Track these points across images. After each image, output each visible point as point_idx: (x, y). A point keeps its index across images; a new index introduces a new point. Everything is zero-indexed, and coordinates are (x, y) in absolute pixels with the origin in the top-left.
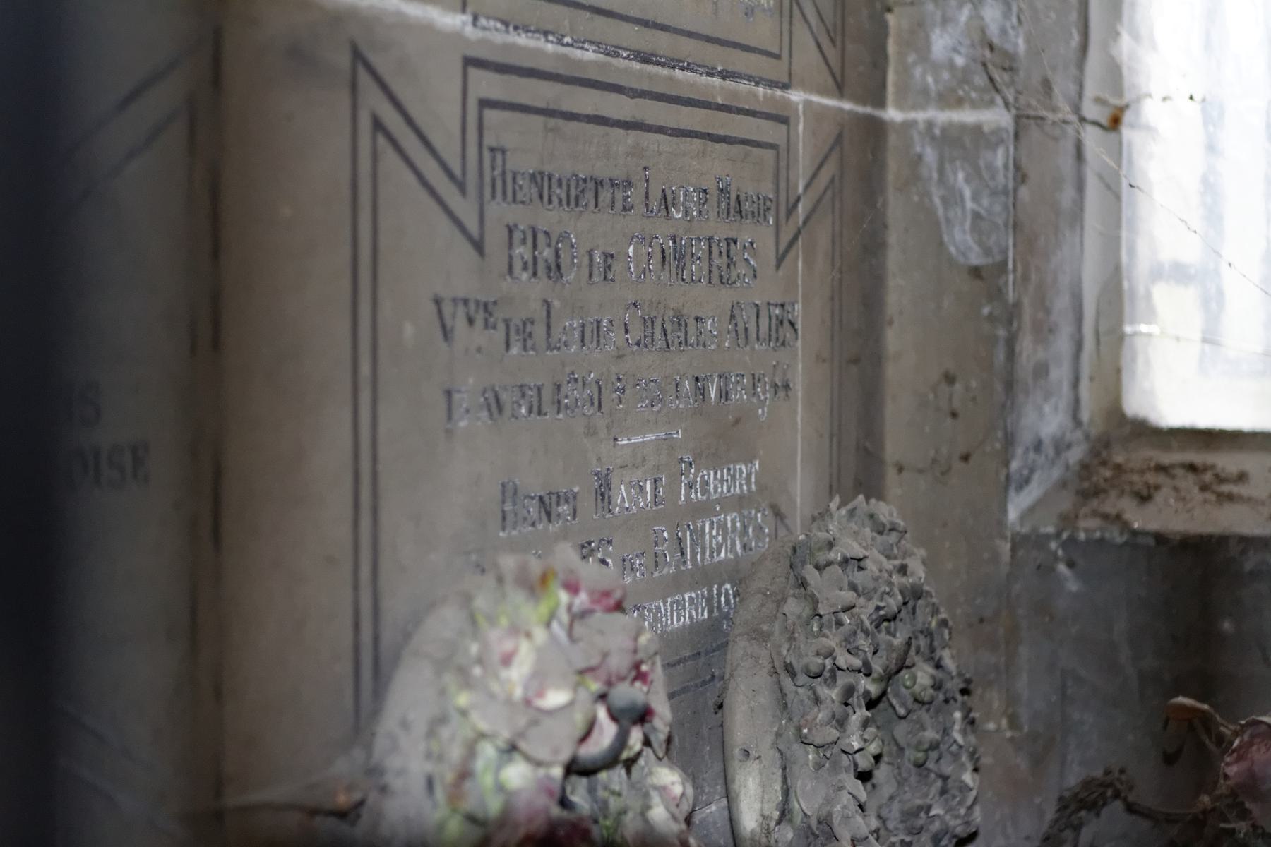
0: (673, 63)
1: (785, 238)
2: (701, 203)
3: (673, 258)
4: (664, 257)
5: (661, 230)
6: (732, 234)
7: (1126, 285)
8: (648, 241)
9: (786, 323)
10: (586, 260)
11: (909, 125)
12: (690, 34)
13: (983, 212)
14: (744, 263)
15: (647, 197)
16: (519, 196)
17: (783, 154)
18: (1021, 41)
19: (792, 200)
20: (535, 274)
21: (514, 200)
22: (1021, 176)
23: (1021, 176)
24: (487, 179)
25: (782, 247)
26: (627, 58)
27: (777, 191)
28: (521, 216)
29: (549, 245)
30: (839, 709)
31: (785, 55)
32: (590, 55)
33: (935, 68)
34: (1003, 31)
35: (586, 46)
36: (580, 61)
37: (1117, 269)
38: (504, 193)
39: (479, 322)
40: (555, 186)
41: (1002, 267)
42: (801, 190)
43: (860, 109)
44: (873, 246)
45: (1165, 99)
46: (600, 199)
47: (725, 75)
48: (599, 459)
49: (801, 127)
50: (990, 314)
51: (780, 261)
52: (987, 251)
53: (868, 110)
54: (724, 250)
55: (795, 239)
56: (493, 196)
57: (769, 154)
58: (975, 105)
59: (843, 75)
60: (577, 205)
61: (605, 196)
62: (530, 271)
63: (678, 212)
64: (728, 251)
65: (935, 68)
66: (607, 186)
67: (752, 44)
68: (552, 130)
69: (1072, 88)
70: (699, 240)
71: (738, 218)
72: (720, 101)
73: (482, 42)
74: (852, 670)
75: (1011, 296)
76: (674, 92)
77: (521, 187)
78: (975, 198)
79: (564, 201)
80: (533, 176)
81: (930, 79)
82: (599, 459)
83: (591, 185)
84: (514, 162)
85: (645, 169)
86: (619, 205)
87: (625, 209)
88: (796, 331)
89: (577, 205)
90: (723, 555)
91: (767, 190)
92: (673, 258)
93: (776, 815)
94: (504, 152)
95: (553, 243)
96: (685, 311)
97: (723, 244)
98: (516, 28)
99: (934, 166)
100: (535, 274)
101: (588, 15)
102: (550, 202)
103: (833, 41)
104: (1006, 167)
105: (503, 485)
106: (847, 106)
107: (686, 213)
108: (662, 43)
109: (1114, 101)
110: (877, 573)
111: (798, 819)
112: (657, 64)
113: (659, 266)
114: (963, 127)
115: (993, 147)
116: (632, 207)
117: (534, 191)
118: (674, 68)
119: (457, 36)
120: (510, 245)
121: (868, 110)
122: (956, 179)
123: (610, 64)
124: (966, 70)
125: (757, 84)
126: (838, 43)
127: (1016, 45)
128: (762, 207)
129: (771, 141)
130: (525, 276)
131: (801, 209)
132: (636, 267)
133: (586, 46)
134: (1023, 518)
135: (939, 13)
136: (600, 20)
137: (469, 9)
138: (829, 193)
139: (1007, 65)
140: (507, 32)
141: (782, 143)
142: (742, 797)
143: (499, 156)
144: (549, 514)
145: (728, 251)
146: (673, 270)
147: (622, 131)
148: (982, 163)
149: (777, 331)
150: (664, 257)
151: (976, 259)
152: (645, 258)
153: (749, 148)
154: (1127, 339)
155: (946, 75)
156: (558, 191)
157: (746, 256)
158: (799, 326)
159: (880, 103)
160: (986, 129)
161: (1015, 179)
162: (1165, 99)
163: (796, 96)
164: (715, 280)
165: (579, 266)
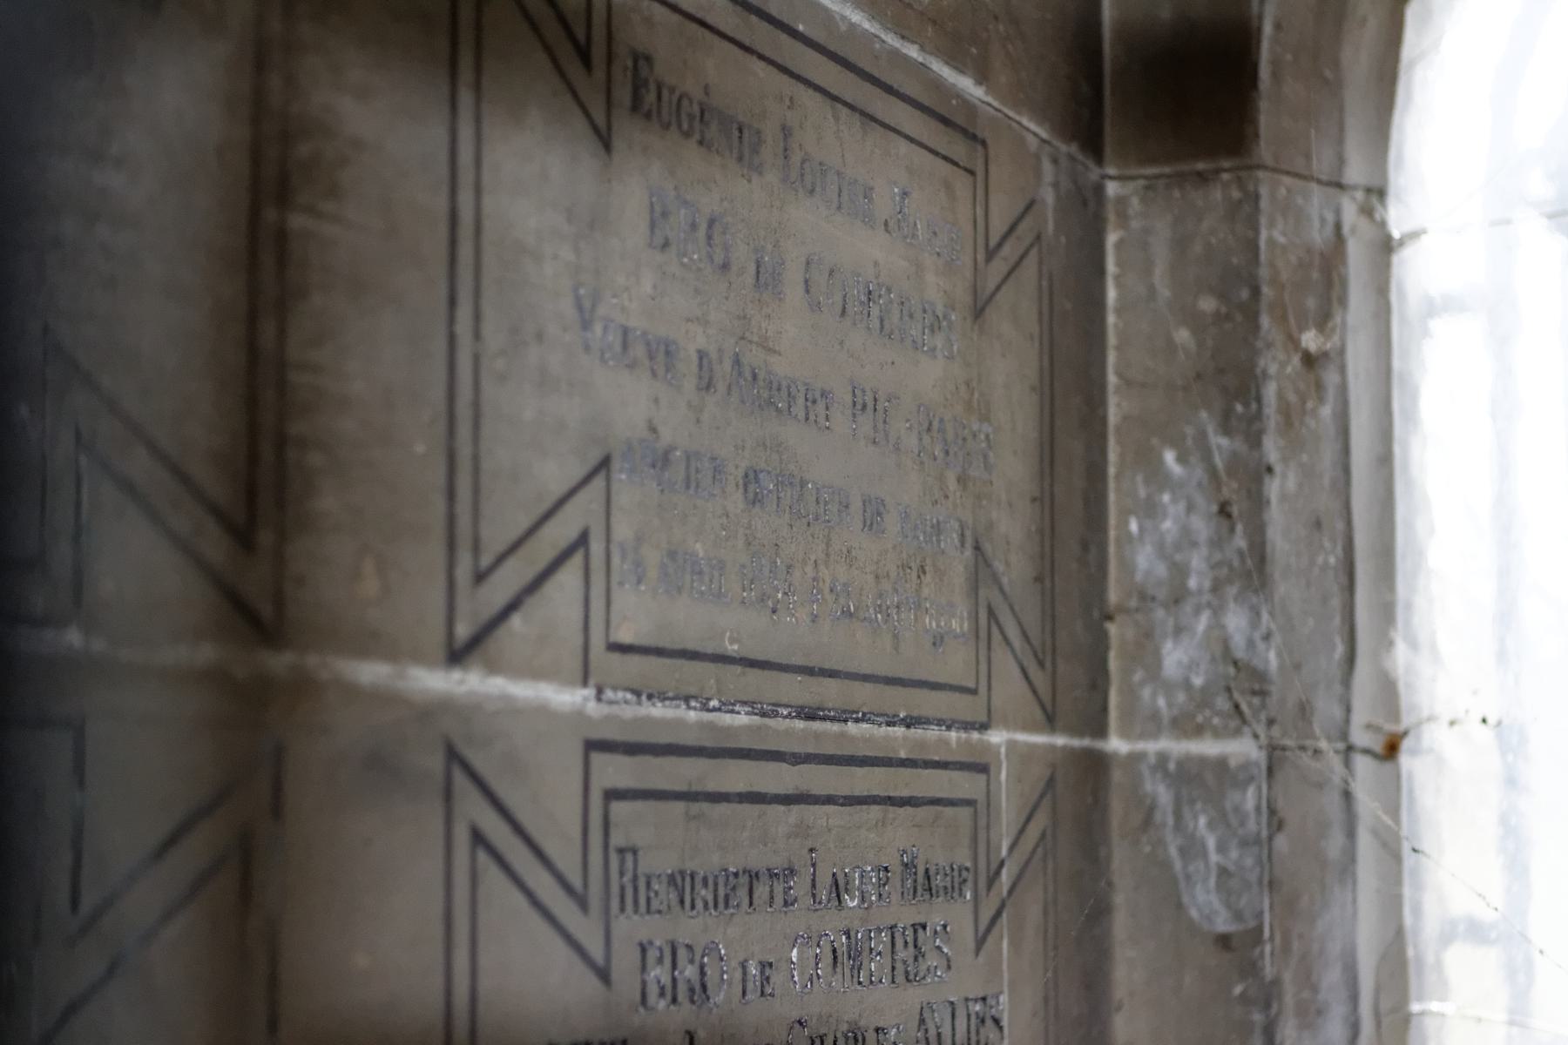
2: (882, 884)
3: (848, 958)
4: (835, 958)
5: (831, 924)
7: (1410, 952)
8: (815, 940)
10: (738, 975)
11: (1136, 758)
12: (866, 678)
13: (1232, 868)
14: (935, 953)
15: (814, 886)
16: (655, 904)
17: (981, 807)
18: (1272, 656)
19: (994, 866)
20: (674, 1000)
21: (648, 911)
22: (1276, 823)
23: (1276, 823)
24: (615, 889)
25: (982, 928)
26: (789, 716)
28: (655, 929)
29: (692, 961)
31: (983, 689)
32: (742, 719)
33: (1168, 688)
34: (1251, 644)
35: (737, 708)
37: (1399, 933)
38: (636, 902)
40: (699, 886)
41: (1256, 935)
42: (1004, 852)
43: (1076, 742)
44: (1098, 912)
45: (1452, 723)
46: (755, 896)
47: (909, 723)
50: (1243, 994)
51: (980, 943)
52: (1238, 916)
53: (1086, 742)
54: (910, 939)
55: (998, 914)
56: (622, 909)
57: (964, 813)
58: (1218, 734)
59: (1054, 705)
60: (727, 905)
61: (761, 891)
62: (669, 996)
63: (852, 899)
64: (916, 940)
65: (1168, 688)
66: (764, 878)
67: (941, 679)
69: (1337, 712)
70: (879, 930)
71: (927, 896)
72: (903, 755)
73: (608, 719)
75: (1269, 971)
76: (847, 751)
77: (656, 893)
78: (1222, 848)
79: (711, 904)
80: (672, 879)
81: (1161, 702)
83: (744, 880)
85: (811, 850)
86: (779, 900)
87: (786, 904)
88: (1001, 1029)
89: (727, 905)
91: (963, 857)
92: (848, 958)
95: (697, 958)
96: (862, 1023)
98: (650, 697)
99: (1170, 809)
100: (674, 1000)
101: (738, 669)
102: (693, 907)
103: (1041, 664)
104: (1258, 809)
106: (1060, 741)
107: (863, 900)
108: (830, 692)
109: (1390, 727)
112: (824, 719)
113: (830, 969)
114: (1203, 761)
115: (1242, 785)
116: (796, 900)
117: (673, 896)
118: (846, 721)
119: (579, 715)
120: (644, 968)
121: (1086, 742)
122: (1196, 827)
123: (768, 727)
124: (1204, 689)
125: (949, 728)
126: (1048, 664)
127: (1267, 661)
128: (956, 880)
129: (967, 796)
130: (662, 1004)
131: (1005, 878)
132: (801, 974)
133: (737, 708)
135: (1171, 622)
136: (754, 675)
137: (592, 681)
139: (1257, 687)
140: (639, 703)
141: (980, 796)
143: (629, 857)
145: (916, 940)
146: (847, 971)
147: (782, 808)
148: (1228, 805)
149: (978, 1032)
150: (835, 958)
151: (1223, 924)
152: (813, 961)
153: (939, 808)
154: (1414, 1022)
155: (1181, 697)
156: (703, 892)
157: (938, 942)
158: (1005, 1023)
159: (1101, 731)
160: (1233, 763)
161: (1269, 825)
162: (1452, 723)
164: (900, 978)
165: (730, 983)
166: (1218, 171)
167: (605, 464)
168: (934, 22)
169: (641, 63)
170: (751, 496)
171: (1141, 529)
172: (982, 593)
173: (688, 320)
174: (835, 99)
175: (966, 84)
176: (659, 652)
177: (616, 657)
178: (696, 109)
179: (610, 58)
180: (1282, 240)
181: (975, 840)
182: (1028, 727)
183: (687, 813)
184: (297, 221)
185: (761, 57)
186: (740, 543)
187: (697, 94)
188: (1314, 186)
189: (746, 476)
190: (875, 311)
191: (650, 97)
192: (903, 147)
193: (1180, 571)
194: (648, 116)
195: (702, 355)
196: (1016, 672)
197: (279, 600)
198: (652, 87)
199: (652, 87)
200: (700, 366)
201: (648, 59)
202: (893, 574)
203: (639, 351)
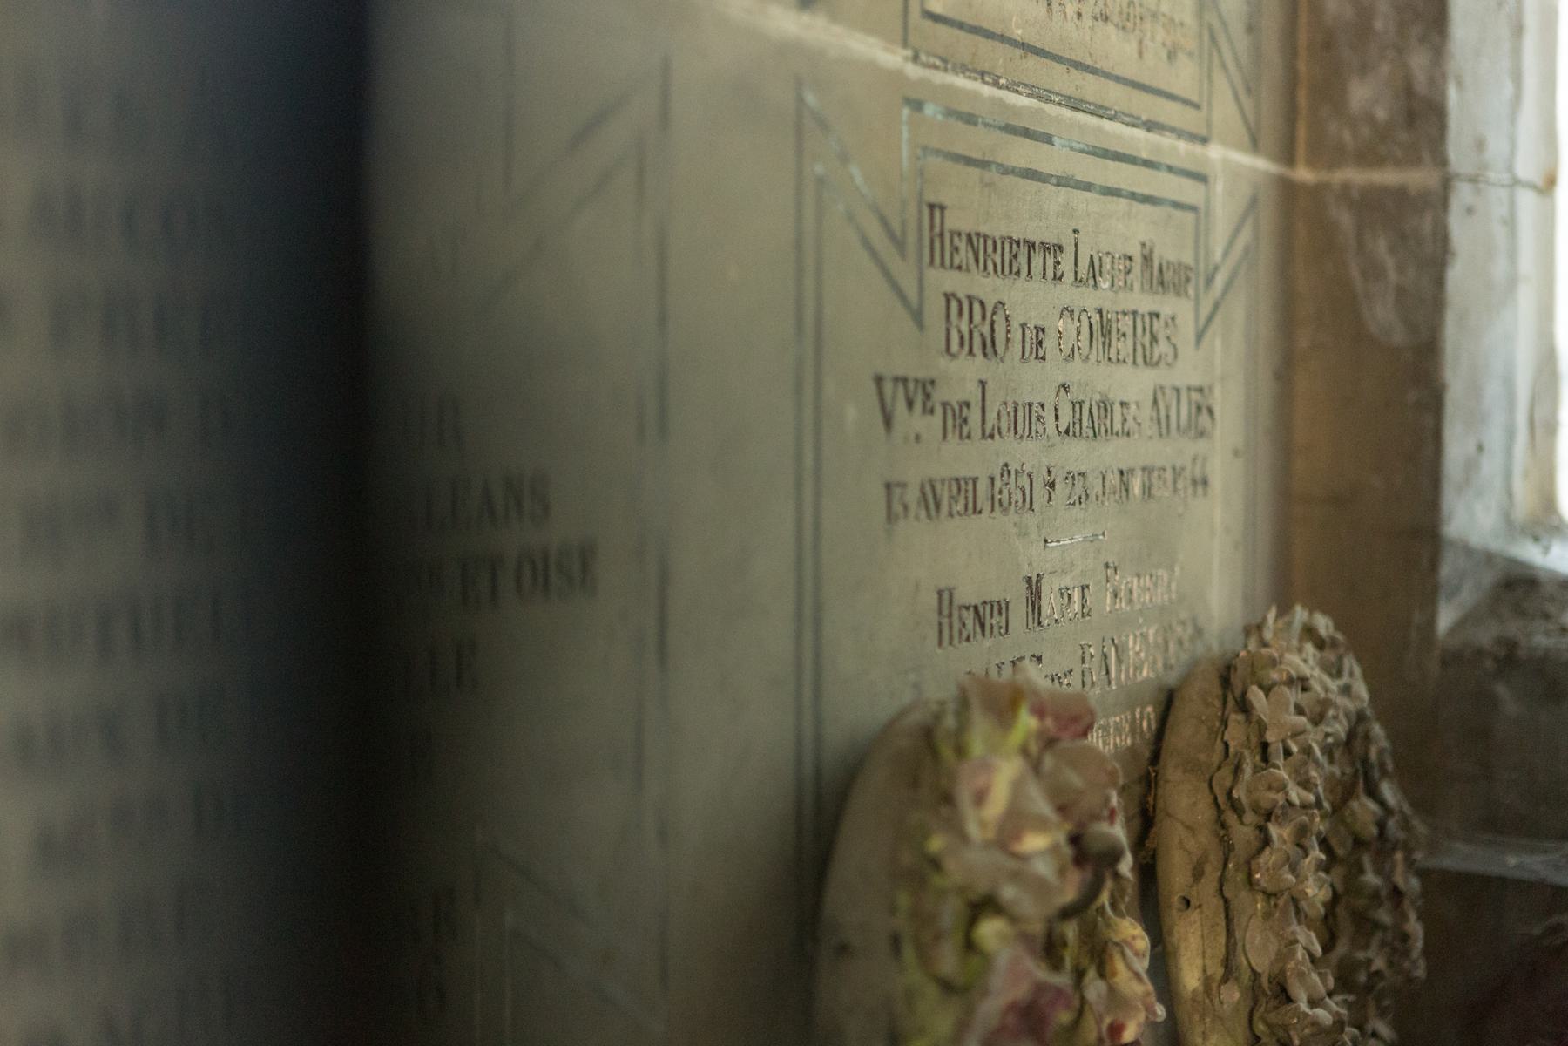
0: (1099, 111)
1: (1205, 311)
5: (1087, 299)
6: (1155, 308)
9: (1205, 411)
12: (1118, 79)
20: (971, 351)
27: (1197, 260)
30: (1290, 848)
31: (1205, 105)
36: (1014, 106)
39: (918, 406)
42: (1218, 253)
48: (1030, 564)
51: (1199, 337)
57: (1189, 217)
58: (1398, 163)
61: (1037, 260)
68: (987, 185)
72: (1144, 155)
74: (1305, 806)
78: (1401, 269)
81: (1347, 136)
82: (1030, 564)
84: (954, 221)
90: (1145, 673)
91: (1187, 258)
93: (1220, 971)
94: (942, 208)
96: (1111, 396)
97: (1147, 319)
103: (1249, 90)
105: (940, 593)
110: (1323, 695)
111: (1246, 977)
114: (1385, 190)
119: (896, 76)
129: (1172, 177)
131: (1220, 281)
134: (1460, 625)
140: (946, 70)
141: (1200, 203)
142: (1182, 951)
144: (983, 626)
155: (1365, 131)
176: (961, 26)
177: (928, 23)
181: (1197, 242)
182: (1238, 147)
183: (981, 180)
196: (1229, 93)
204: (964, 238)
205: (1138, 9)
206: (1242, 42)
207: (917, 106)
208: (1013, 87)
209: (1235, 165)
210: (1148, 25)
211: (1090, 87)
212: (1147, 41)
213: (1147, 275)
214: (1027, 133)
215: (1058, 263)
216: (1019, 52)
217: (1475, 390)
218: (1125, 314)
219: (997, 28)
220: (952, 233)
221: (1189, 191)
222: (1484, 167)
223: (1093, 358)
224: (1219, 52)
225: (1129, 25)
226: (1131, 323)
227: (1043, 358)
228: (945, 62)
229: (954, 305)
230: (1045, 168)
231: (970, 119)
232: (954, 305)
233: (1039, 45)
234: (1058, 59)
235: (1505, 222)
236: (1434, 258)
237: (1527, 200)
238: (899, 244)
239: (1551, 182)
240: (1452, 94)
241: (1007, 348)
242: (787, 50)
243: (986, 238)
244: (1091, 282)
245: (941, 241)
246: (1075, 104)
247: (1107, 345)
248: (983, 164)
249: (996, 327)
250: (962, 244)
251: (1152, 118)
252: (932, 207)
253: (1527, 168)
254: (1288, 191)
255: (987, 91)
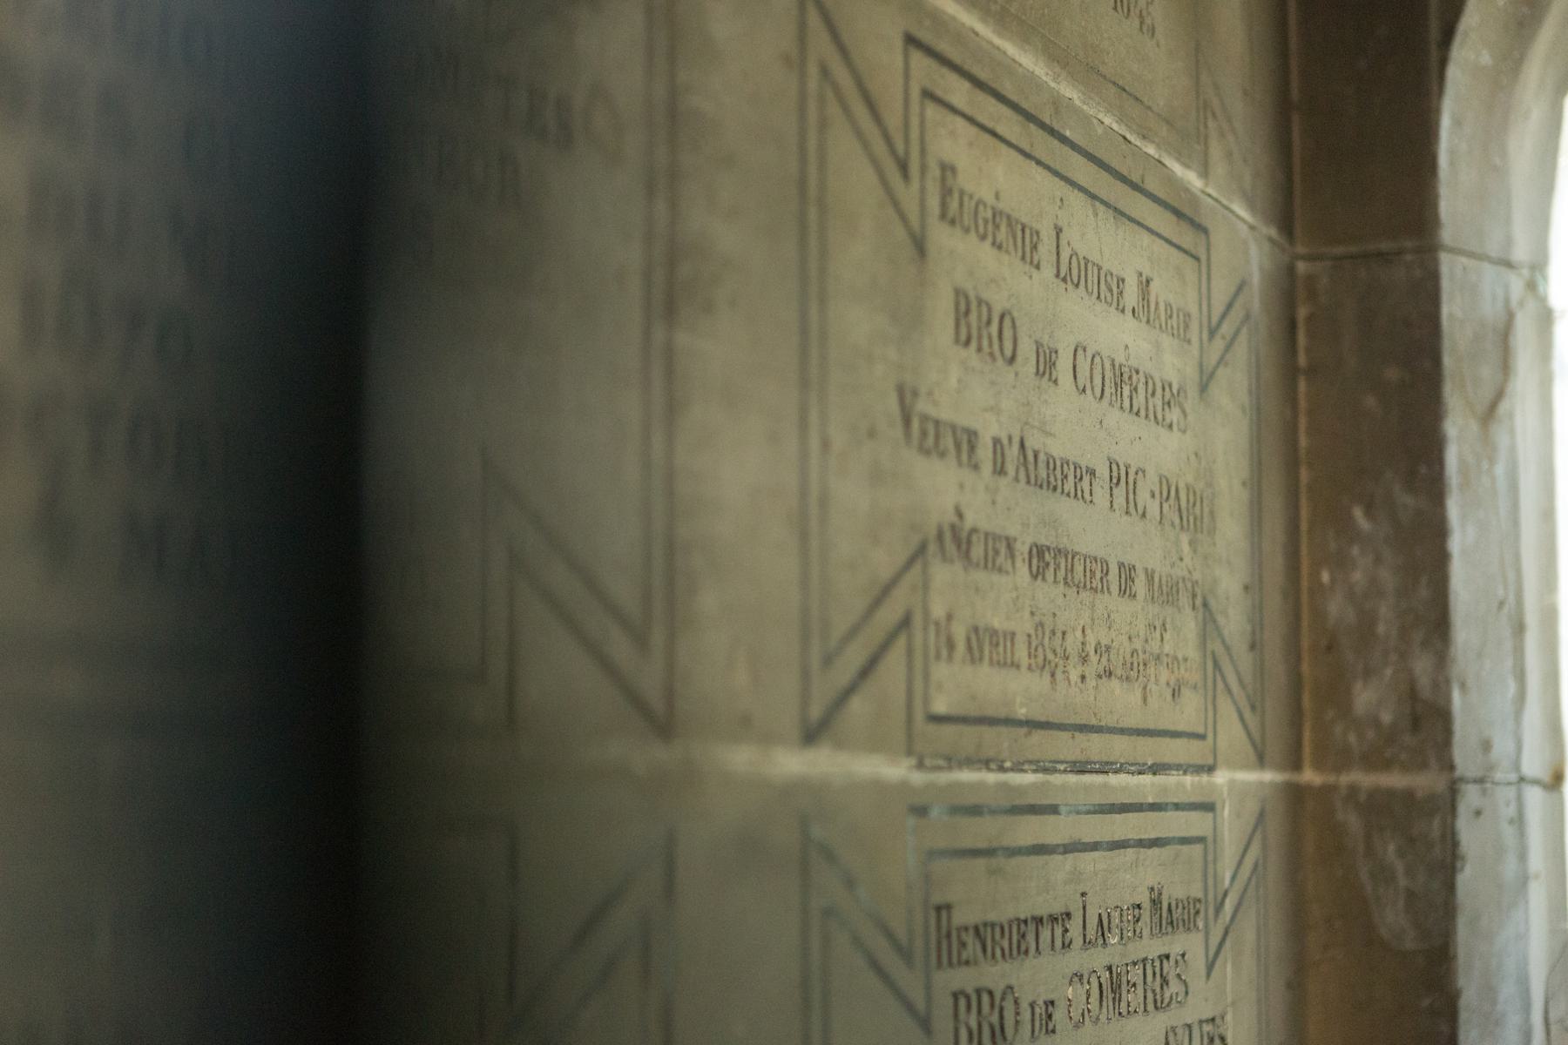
0: (1105, 768)
1: (1214, 941)
5: (1098, 959)
12: (1122, 731)
17: (1210, 839)
25: (1212, 953)
26: (1065, 771)
27: (1206, 895)
49: (1226, 812)
51: (1210, 968)
54: (1158, 970)
57: (1197, 849)
58: (1406, 768)
61: (1045, 934)
67: (1180, 728)
72: (1150, 800)
81: (1352, 738)
84: (961, 917)
86: (1058, 943)
94: (948, 907)
97: (1157, 964)
103: (1253, 708)
114: (1391, 793)
119: (904, 787)
125: (1185, 773)
129: (1180, 813)
138: (1253, 882)
141: (1208, 833)
155: (1371, 734)
160: (1420, 794)
163: (1221, 777)
164: (1150, 1007)
166: (1399, 253)
167: (922, 549)
168: (1168, 122)
169: (949, 173)
170: (1034, 569)
171: (1333, 580)
172: (1210, 647)
173: (986, 410)
174: (1094, 197)
175: (1193, 179)
177: (932, 728)
178: (989, 214)
179: (924, 169)
180: (1459, 314)
182: (1245, 767)
184: (682, 339)
185: (1039, 163)
186: (1027, 614)
187: (989, 198)
188: (1486, 266)
189: (1030, 552)
190: (1126, 392)
191: (954, 205)
192: (1146, 238)
193: (1367, 622)
194: (953, 222)
195: (996, 441)
197: (670, 695)
198: (956, 195)
199: (956, 195)
200: (995, 452)
201: (953, 170)
202: (1142, 633)
203: (948, 442)
204: (971, 931)
205: (1141, 656)
206: (1246, 660)
207: (921, 811)
208: (1018, 768)
209: (1241, 783)
210: (1151, 670)
211: (1095, 747)
212: (1152, 686)
213: (1156, 919)
214: (1034, 810)
215: (1066, 931)
216: (1024, 730)
217: (1489, 991)
218: (1135, 964)
219: (1002, 713)
220: (959, 930)
221: (1196, 824)
222: (1491, 768)
223: (1103, 1018)
224: (1223, 677)
225: (1133, 674)
226: (1140, 972)
227: (1053, 1031)
228: (953, 761)
229: (962, 1002)
230: (1052, 839)
231: (975, 811)
232: (962, 1002)
233: (1043, 719)
234: (1061, 727)
235: (1511, 822)
236: (1444, 862)
237: (1534, 796)
238: (906, 954)
239: (1558, 778)
240: (1456, 696)
241: (1016, 1030)
242: (792, 790)
243: (993, 925)
244: (1100, 941)
245: (949, 938)
246: (1080, 768)
247: (1117, 1000)
248: (989, 852)
249: (1006, 1013)
250: (970, 939)
251: (1158, 761)
252: (938, 909)
253: (1533, 764)
254: (1295, 795)
255: (991, 777)
